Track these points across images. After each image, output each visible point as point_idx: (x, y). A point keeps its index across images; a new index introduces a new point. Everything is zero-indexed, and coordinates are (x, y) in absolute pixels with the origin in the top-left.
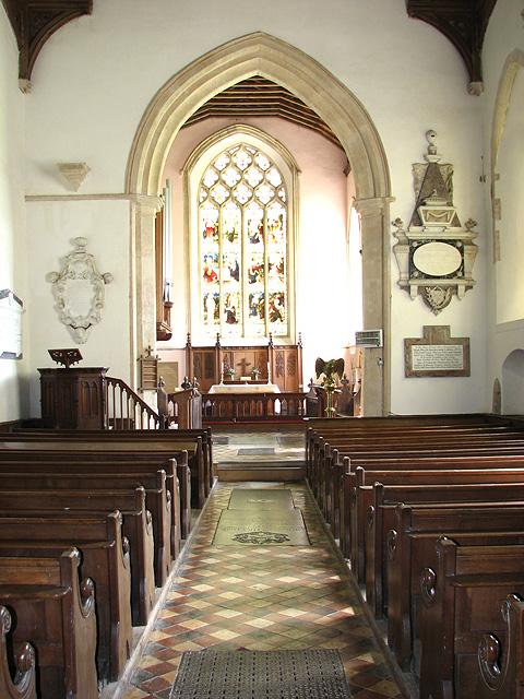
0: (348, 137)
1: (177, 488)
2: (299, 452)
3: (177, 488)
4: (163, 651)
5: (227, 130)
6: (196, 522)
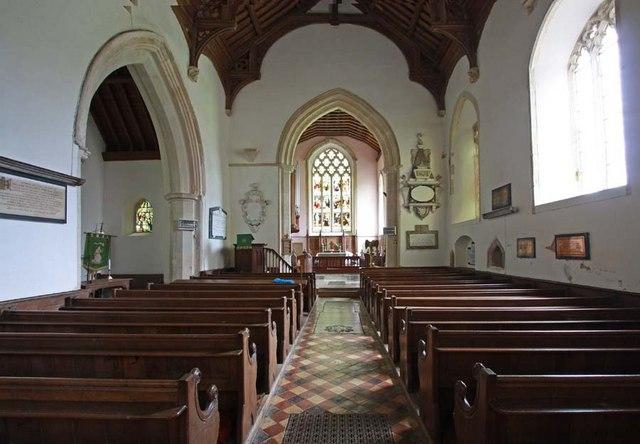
0: (380, 139)
1: (294, 305)
2: (357, 284)
3: (294, 305)
4: (277, 413)
5: (326, 141)
6: (305, 320)
